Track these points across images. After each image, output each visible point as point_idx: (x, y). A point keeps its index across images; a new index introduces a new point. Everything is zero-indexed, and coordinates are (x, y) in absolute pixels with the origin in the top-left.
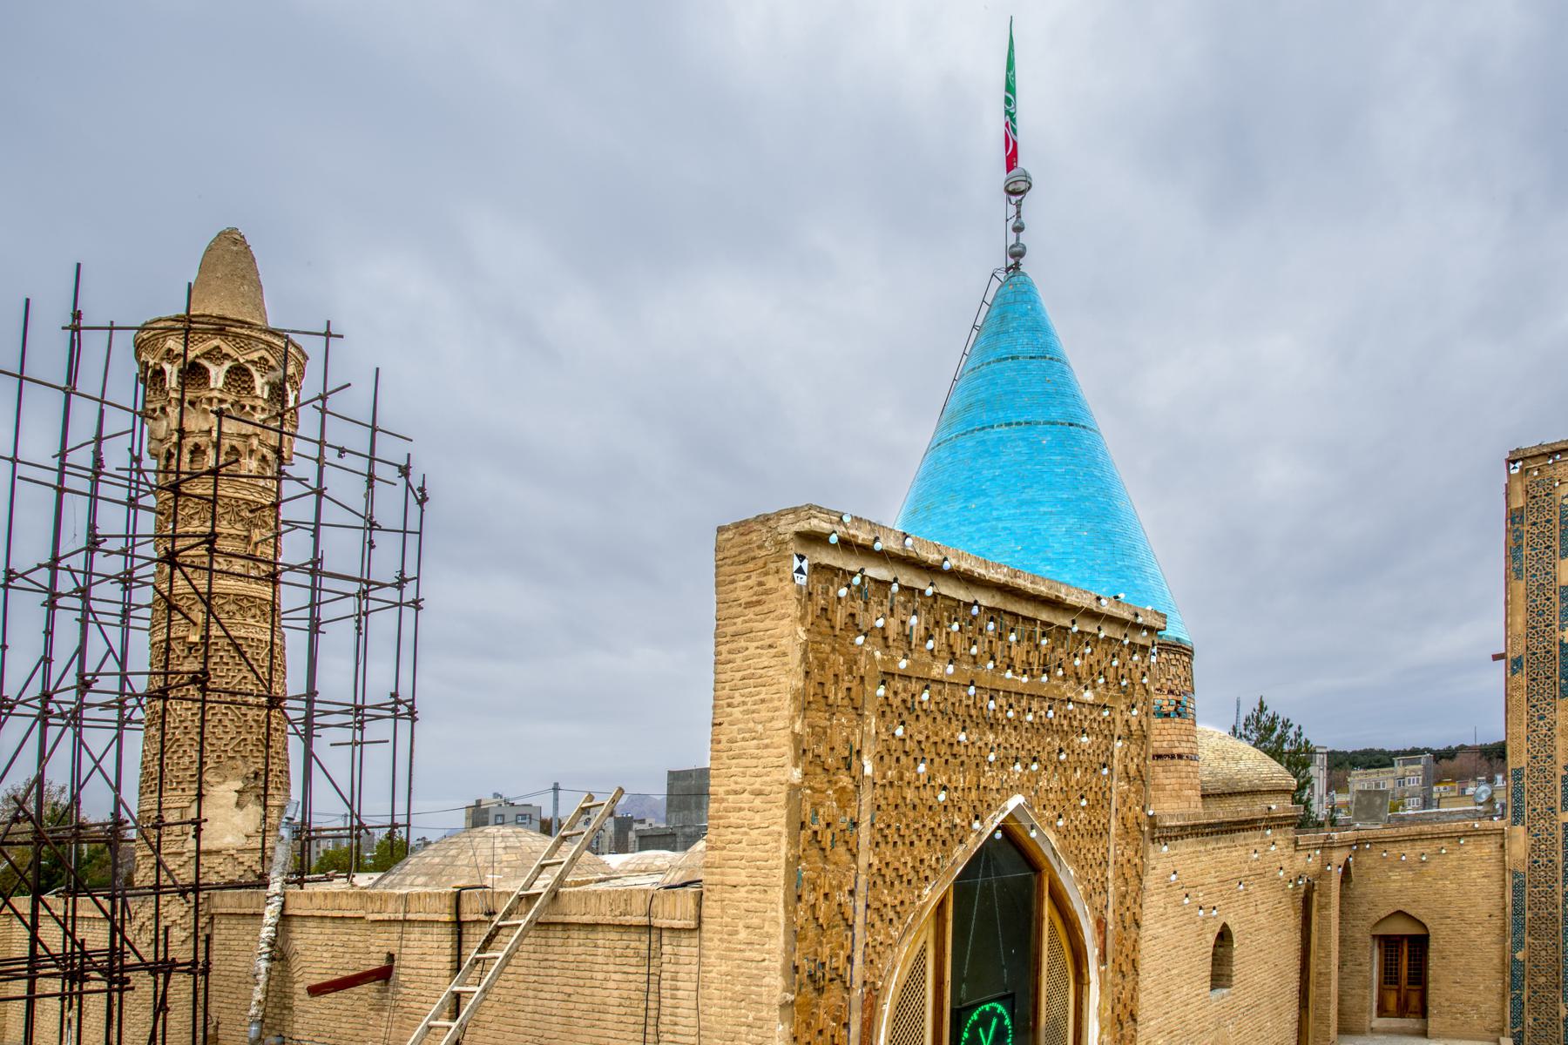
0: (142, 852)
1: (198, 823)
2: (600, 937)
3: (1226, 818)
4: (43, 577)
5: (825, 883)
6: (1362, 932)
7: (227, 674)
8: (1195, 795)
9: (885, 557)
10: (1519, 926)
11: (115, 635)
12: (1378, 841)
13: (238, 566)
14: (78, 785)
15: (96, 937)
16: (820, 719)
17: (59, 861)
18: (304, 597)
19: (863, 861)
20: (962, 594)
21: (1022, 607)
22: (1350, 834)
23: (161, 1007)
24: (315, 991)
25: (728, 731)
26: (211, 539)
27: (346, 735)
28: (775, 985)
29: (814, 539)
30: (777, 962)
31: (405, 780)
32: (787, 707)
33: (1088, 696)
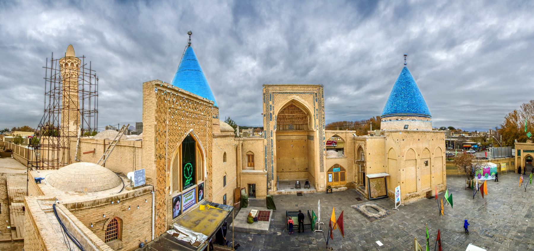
0: (61, 131)
1: (68, 127)
2: (126, 148)
3: (224, 135)
4: (49, 93)
5: (161, 141)
6: (245, 154)
7: (72, 106)
8: (220, 131)
9: (169, 89)
10: (266, 153)
11: (58, 101)
12: (246, 140)
13: (73, 90)
14: (54, 121)
15: (56, 143)
16: (160, 114)
17: (52, 132)
18: (82, 95)
19: (167, 138)
20: (182, 96)
21: (191, 99)
22: (243, 139)
23: (64, 154)
24: (84, 153)
25: (145, 115)
26: (69, 87)
27: (88, 115)
28: (153, 158)
29: (158, 85)
30: (154, 154)
31: (96, 122)
32: (154, 112)
33: (202, 114)
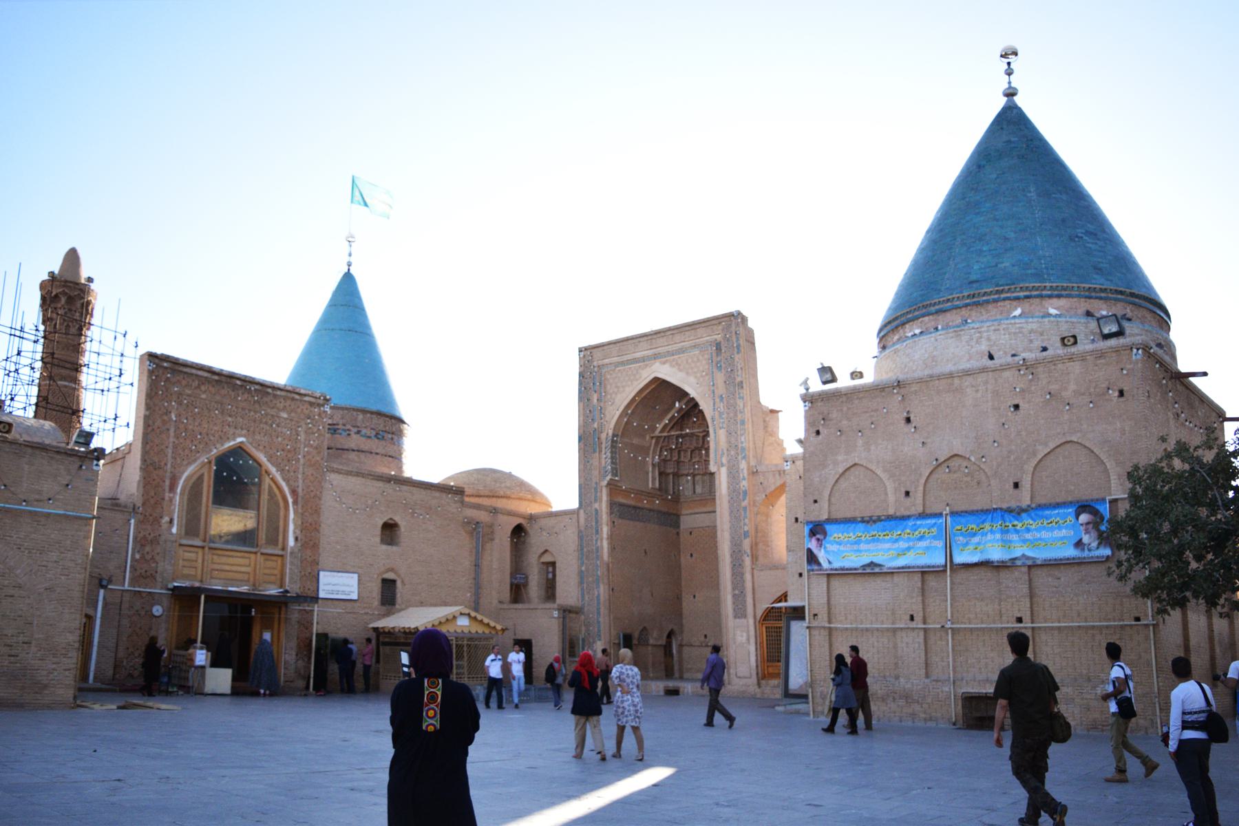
19: (172, 440)
